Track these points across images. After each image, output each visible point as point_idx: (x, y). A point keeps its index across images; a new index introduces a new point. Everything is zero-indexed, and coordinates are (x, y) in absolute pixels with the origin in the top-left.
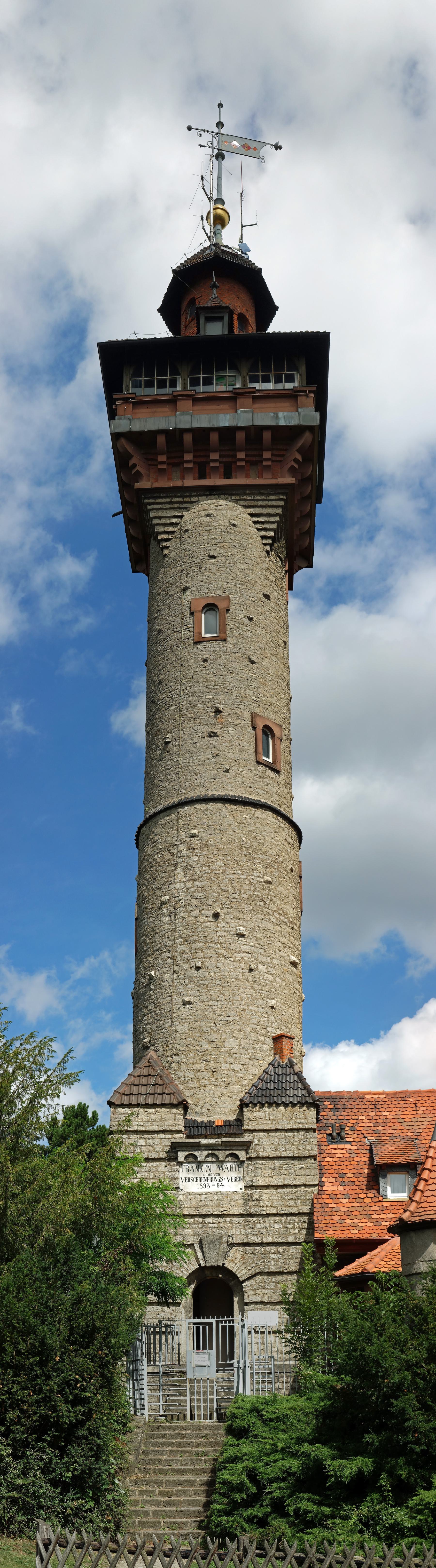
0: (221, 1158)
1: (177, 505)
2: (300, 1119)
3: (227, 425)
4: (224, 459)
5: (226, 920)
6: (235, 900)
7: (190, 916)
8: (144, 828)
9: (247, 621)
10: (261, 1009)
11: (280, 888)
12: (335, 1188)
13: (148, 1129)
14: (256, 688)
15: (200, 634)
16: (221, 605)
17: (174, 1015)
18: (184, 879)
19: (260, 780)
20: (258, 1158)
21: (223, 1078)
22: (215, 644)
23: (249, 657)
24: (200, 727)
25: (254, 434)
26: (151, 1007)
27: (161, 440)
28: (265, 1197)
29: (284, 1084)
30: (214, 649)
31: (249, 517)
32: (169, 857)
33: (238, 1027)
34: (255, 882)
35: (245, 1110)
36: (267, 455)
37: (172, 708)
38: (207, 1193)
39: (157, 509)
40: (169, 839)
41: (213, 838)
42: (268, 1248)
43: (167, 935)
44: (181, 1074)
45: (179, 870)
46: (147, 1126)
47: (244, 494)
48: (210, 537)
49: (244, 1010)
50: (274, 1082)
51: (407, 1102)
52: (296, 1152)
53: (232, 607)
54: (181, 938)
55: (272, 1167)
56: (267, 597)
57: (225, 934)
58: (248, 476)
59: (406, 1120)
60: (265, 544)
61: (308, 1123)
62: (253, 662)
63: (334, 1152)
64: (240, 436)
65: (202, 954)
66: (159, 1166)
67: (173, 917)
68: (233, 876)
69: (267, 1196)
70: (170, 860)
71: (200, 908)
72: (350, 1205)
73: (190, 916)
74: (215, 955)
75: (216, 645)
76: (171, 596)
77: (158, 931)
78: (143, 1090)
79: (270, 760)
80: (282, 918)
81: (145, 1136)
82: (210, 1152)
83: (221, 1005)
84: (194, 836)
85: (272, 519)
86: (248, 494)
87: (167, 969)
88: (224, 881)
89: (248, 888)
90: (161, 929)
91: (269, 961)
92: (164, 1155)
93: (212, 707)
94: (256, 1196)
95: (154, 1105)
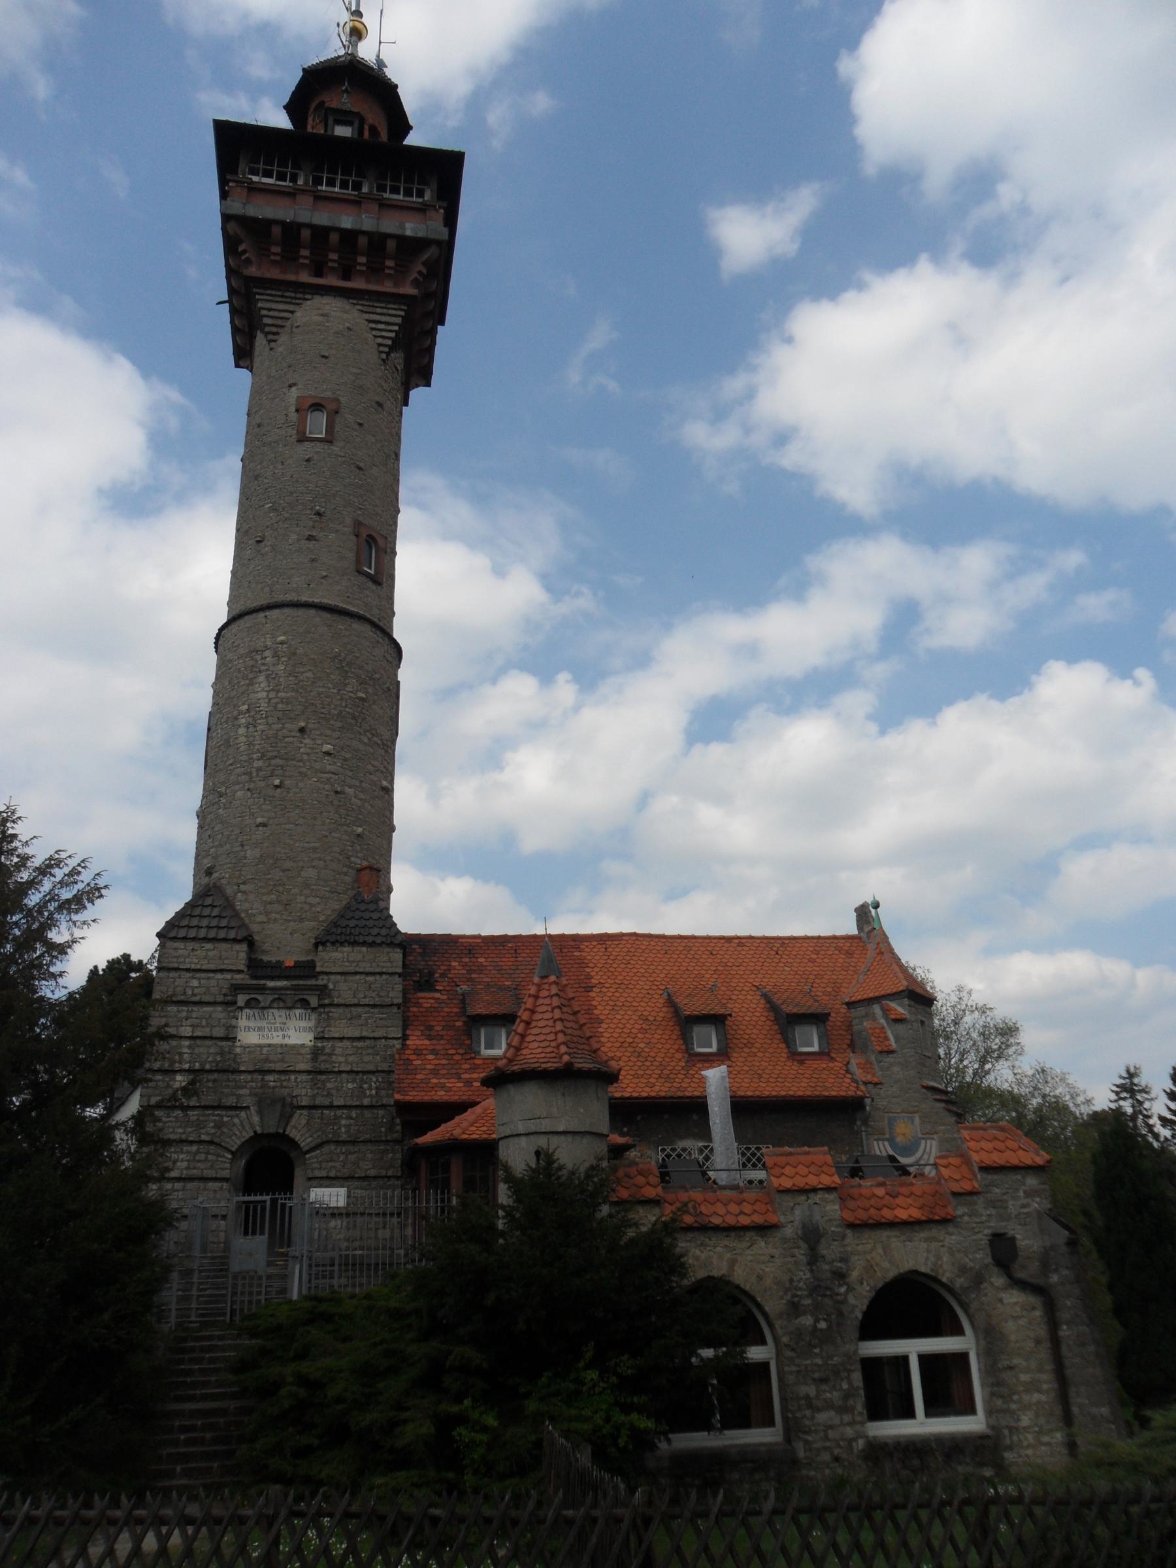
1: (289, 300)
9: (357, 427)
13: (203, 968)
20: (331, 1005)
27: (276, 231)
28: (338, 1051)
33: (317, 855)
38: (269, 1045)
42: (339, 1113)
45: (261, 678)
47: (363, 299)
63: (420, 1001)
64: (363, 241)
69: (341, 1050)
81: (198, 975)
82: (277, 996)
85: (390, 328)
86: (367, 300)
90: (237, 741)
92: (220, 999)
94: (327, 1051)
95: (214, 940)
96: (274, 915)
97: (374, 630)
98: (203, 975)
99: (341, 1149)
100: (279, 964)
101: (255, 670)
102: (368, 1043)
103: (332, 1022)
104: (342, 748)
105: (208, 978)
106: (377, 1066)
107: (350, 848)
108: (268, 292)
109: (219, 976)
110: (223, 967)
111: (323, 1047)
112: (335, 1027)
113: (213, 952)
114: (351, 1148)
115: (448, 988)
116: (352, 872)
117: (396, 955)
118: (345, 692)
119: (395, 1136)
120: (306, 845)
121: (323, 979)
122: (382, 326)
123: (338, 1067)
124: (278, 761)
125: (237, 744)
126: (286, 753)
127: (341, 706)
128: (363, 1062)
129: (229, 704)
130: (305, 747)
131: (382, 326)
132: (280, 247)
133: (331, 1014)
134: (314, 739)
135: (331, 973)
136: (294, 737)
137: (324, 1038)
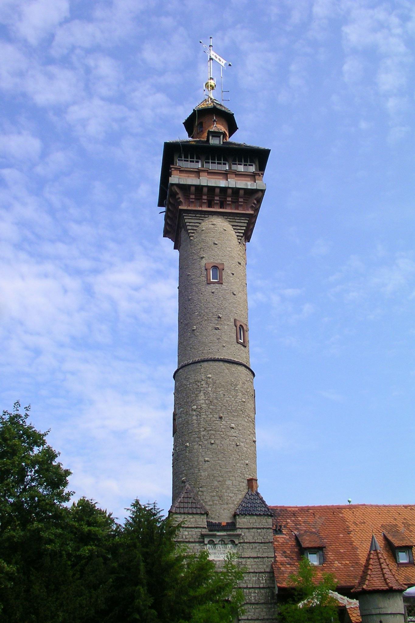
0: (226, 542)
1: (198, 218)
2: (264, 523)
3: (224, 186)
4: (221, 199)
5: (225, 420)
6: (229, 411)
7: (207, 417)
8: (181, 370)
9: (231, 275)
10: (242, 466)
11: (248, 404)
12: (282, 559)
13: (189, 526)
14: (236, 307)
15: (210, 280)
16: (220, 267)
17: (200, 466)
18: (205, 399)
19: (238, 351)
20: (244, 542)
21: (225, 500)
22: (217, 285)
23: (233, 293)
24: (211, 324)
25: (236, 191)
26: (187, 461)
27: (193, 189)
28: (248, 563)
29: (251, 504)
30: (217, 287)
31: (231, 226)
32: (196, 387)
33: (232, 475)
34: (238, 402)
35: (237, 517)
36: (241, 200)
37: (196, 313)
38: (219, 561)
39: (189, 219)
40: (196, 378)
41: (219, 379)
42: (250, 590)
43: (195, 426)
44: (204, 498)
45: (202, 394)
46: (189, 525)
47: (230, 216)
48: (214, 235)
49: (235, 466)
50: (250, 503)
51: (309, 512)
52: (262, 540)
53: (225, 268)
54: (203, 428)
55: (251, 547)
56: (240, 264)
57: (225, 427)
58: (231, 209)
59: (311, 522)
60: (238, 239)
61: (268, 525)
62: (235, 295)
63: (278, 539)
64: (230, 191)
65: (214, 437)
66: (195, 546)
67: (199, 417)
68: (228, 399)
69: (249, 563)
70: (197, 388)
71: (212, 414)
72: (291, 568)
73: (207, 417)
74: (220, 438)
75: (217, 286)
76: (195, 259)
77: (190, 423)
78: (186, 505)
79: (242, 341)
80: (249, 419)
81: (188, 529)
82: (221, 539)
83: (224, 463)
84: (209, 378)
85: (242, 228)
86: (232, 216)
87: (196, 443)
88: (224, 401)
89: (235, 404)
90: (192, 422)
91: (245, 441)
92: (197, 540)
93: (216, 315)
94: (244, 563)
95: (193, 514)
96: (215, 502)
97: (246, 369)
98: (190, 530)
99: (253, 607)
100: (220, 524)
101: (198, 390)
102: (260, 559)
103: (245, 550)
104: (238, 425)
105: (191, 531)
106: (265, 570)
107: (244, 470)
108: (189, 215)
109: (197, 530)
110: (198, 526)
111: (242, 561)
112: (246, 552)
113: (193, 519)
114: (256, 606)
115: (288, 533)
116: (246, 482)
117: (269, 520)
118: (237, 399)
119: (274, 601)
120: (227, 470)
121: (239, 531)
122: (239, 228)
123: (249, 570)
124: (213, 432)
125: (193, 424)
126: (215, 428)
127: (236, 406)
128: (259, 568)
129: (187, 405)
130: (223, 425)
131: (239, 228)
132: (194, 196)
133: (244, 547)
134: (226, 422)
135: (242, 528)
136: (218, 421)
137: (241, 557)
